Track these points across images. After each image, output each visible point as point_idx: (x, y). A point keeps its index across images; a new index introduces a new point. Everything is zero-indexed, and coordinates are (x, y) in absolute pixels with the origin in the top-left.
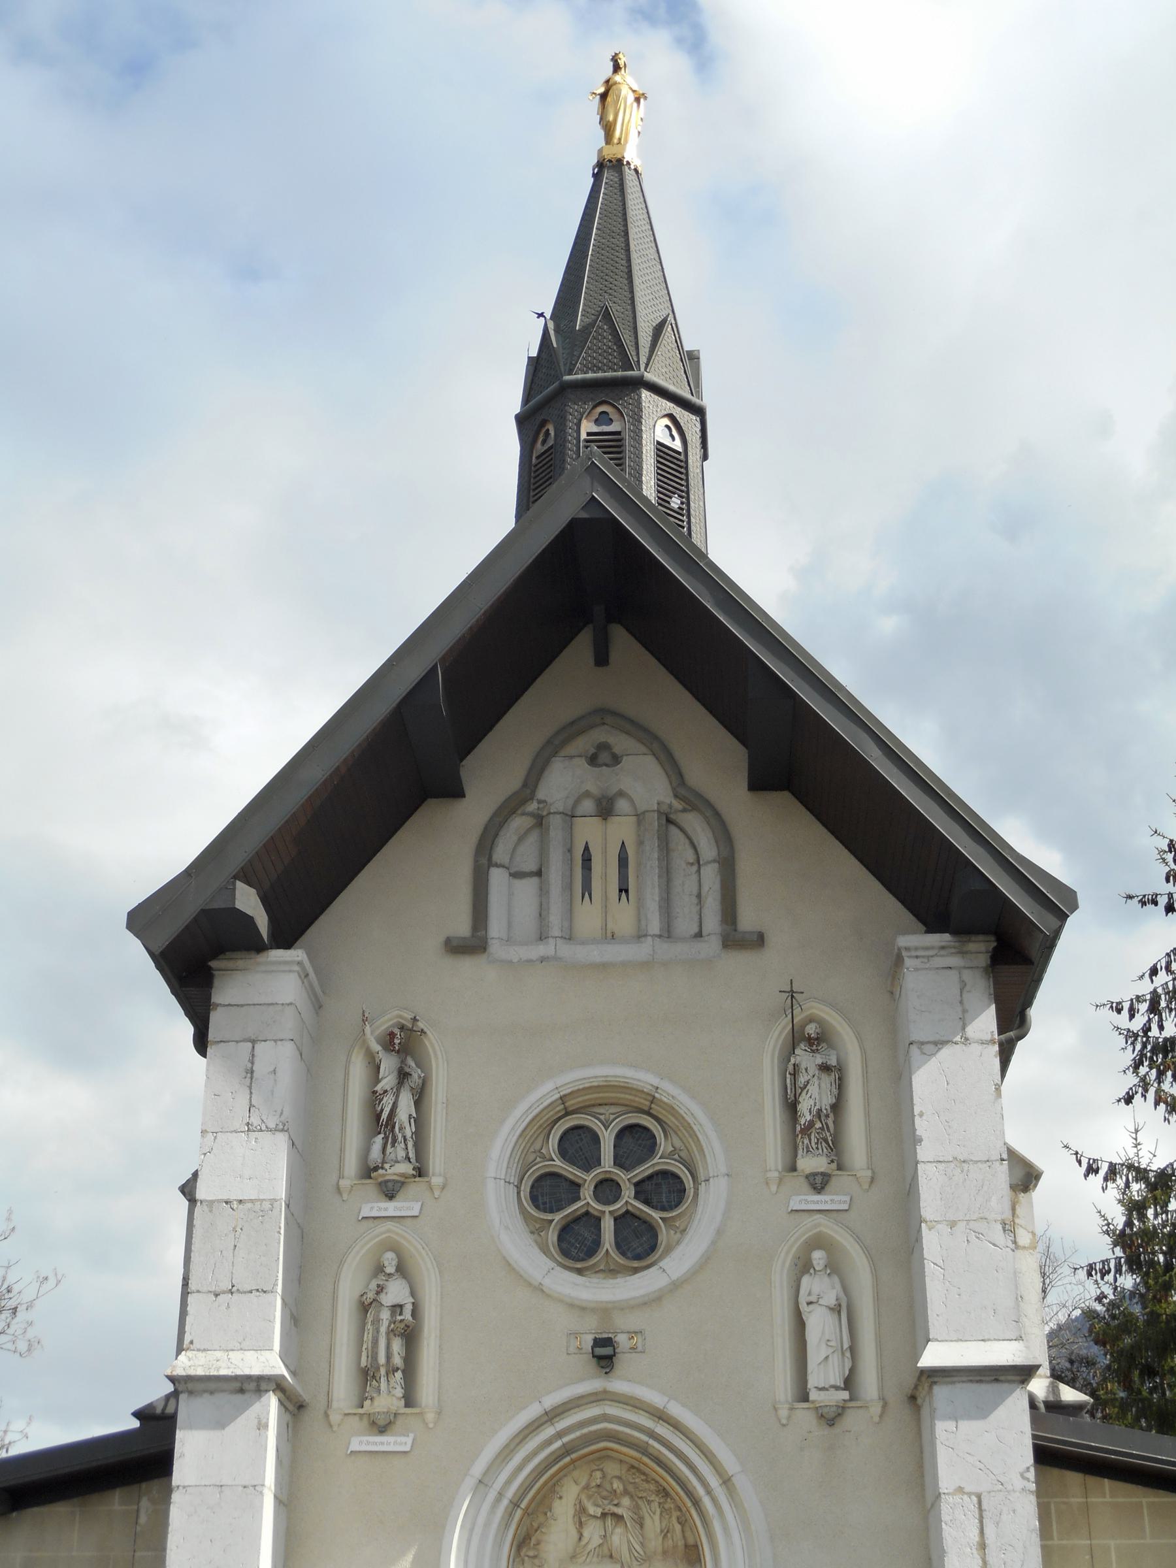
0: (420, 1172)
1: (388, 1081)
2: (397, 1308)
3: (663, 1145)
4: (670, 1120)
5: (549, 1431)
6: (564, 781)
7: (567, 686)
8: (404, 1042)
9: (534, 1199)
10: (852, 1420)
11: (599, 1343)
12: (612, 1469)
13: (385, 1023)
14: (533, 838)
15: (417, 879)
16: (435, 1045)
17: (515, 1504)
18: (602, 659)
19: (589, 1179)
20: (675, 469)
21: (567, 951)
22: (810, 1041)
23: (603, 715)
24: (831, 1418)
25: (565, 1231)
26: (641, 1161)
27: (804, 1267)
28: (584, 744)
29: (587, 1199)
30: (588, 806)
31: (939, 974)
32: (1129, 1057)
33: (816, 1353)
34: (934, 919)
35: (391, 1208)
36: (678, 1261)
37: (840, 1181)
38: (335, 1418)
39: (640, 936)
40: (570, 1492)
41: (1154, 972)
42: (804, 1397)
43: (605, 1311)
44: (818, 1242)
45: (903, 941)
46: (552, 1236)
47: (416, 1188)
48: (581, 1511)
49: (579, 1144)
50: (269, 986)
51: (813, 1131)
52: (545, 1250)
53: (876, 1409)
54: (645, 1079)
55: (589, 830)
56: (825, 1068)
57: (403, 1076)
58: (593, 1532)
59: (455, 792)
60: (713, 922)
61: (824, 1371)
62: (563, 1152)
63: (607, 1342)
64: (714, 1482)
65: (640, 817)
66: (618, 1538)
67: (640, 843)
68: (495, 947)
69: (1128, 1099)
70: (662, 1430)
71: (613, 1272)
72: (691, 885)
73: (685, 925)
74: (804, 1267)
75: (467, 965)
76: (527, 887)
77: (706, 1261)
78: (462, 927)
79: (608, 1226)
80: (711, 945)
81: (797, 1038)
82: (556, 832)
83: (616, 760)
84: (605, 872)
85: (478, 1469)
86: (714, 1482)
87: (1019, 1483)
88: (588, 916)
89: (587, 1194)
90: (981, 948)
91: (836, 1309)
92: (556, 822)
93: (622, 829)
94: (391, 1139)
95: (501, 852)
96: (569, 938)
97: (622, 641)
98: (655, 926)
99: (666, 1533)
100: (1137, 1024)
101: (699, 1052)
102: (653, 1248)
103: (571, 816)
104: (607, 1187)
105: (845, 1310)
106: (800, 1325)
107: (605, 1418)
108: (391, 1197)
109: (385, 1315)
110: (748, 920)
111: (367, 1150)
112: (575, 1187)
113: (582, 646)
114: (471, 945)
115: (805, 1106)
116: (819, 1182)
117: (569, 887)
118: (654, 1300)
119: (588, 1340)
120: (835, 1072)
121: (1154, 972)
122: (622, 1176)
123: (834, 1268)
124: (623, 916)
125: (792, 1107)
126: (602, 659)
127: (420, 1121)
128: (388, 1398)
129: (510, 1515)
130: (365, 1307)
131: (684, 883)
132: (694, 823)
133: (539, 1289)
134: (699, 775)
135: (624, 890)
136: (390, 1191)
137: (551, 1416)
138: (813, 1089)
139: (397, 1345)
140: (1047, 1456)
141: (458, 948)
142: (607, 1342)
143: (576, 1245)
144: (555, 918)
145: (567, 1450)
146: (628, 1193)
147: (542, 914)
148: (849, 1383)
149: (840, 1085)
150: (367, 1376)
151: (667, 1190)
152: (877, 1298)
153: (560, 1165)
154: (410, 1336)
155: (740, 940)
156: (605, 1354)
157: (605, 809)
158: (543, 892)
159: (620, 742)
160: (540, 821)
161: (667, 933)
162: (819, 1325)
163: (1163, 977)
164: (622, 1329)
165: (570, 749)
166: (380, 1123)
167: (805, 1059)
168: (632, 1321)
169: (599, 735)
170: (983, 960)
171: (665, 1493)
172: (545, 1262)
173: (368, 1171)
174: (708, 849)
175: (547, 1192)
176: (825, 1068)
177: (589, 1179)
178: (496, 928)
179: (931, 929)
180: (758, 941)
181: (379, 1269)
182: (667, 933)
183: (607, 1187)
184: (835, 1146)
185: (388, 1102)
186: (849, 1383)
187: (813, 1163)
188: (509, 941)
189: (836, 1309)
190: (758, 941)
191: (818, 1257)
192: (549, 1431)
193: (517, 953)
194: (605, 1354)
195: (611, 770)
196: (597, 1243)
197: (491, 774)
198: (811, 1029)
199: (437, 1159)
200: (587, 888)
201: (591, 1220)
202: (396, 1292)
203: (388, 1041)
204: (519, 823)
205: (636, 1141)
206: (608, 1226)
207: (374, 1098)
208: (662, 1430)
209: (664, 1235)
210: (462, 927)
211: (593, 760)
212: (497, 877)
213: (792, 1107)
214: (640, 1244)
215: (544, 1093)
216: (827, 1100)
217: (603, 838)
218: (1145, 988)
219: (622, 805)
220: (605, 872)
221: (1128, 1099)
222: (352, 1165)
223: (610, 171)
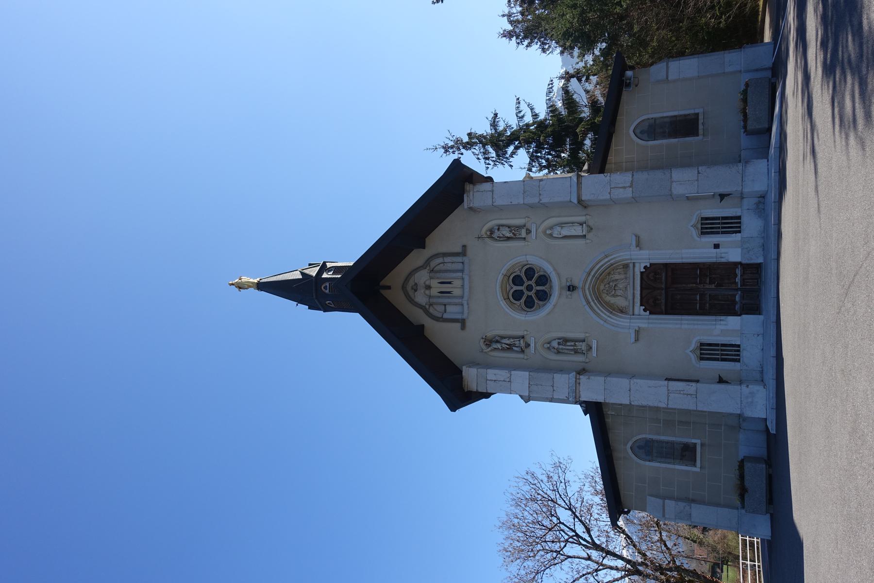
0: (523, 337)
1: (499, 346)
2: (559, 344)
3: (518, 273)
4: (511, 271)
5: (592, 303)
6: (421, 298)
7: (396, 297)
8: (489, 342)
9: (531, 307)
10: (591, 224)
11: (569, 290)
12: (602, 287)
13: (484, 347)
14: (435, 306)
15: (444, 337)
16: (490, 334)
17: (611, 313)
18: (389, 288)
19: (526, 293)
20: (337, 270)
21: (466, 298)
22: (491, 234)
23: (404, 287)
24: (590, 229)
25: (540, 299)
26: (522, 279)
27: (551, 235)
28: (411, 293)
29: (532, 293)
30: (427, 292)
31: (475, 197)
32: (500, 166)
33: (573, 233)
34: (458, 200)
35: (532, 345)
36: (549, 269)
37: (528, 226)
38: (587, 360)
39: (463, 279)
40: (608, 298)
41: (478, 159)
42: (585, 236)
43: (561, 288)
44: (544, 232)
45: (466, 207)
46: (541, 303)
47: (527, 339)
48: (614, 296)
49: (517, 295)
50: (472, 377)
51: (515, 234)
52: (544, 305)
53: (588, 217)
54: (500, 277)
55: (434, 292)
56: (498, 229)
57: (497, 342)
58: (619, 293)
59: (423, 326)
60: (459, 259)
61: (578, 231)
62: (519, 300)
63: (569, 287)
64: (606, 260)
65: (431, 278)
66: (621, 286)
67: (438, 278)
68: (464, 317)
69: (511, 166)
70: (592, 274)
71: (551, 287)
72: (449, 265)
73: (460, 266)
74: (551, 235)
75: (468, 324)
76: (449, 308)
77: (551, 264)
78: (458, 325)
79: (539, 288)
80: (465, 259)
81: (491, 237)
82: (435, 300)
83: (416, 284)
84: (445, 288)
85: (602, 322)
86: (606, 260)
87: (608, 178)
88: (457, 292)
89: (530, 294)
90: (468, 187)
91: (562, 227)
92: (432, 300)
93: (434, 283)
94: (514, 345)
95: (440, 315)
96: (462, 297)
97: (385, 282)
98: (460, 274)
99: (619, 274)
100: (492, 163)
101: (492, 265)
102: (544, 276)
103: (430, 297)
104: (529, 288)
105: (561, 225)
106: (565, 237)
107: (589, 289)
108: (529, 345)
109: (561, 347)
110: (458, 249)
111: (517, 352)
112: (529, 297)
113: (385, 293)
114: (463, 323)
115: (508, 235)
116: (529, 232)
117: (449, 297)
118: (558, 275)
119: (568, 293)
120: (499, 227)
121: (478, 159)
122: (526, 284)
123: (551, 228)
124: (457, 283)
125: (509, 239)
126: (389, 288)
127: (509, 337)
128: (583, 346)
129: (614, 314)
130: (558, 352)
131: (449, 266)
132: (433, 263)
133: (555, 306)
134: (420, 262)
135: (450, 283)
136: (528, 345)
137: (588, 303)
138: (504, 233)
139: (568, 344)
140: (602, 171)
141: (463, 327)
142: (569, 287)
143: (544, 296)
144: (457, 301)
145: (597, 299)
146: (530, 283)
147: (456, 304)
148: (581, 224)
149: (503, 226)
150: (576, 352)
151: (530, 272)
152: (559, 216)
153: (523, 300)
154: (566, 340)
155: (463, 253)
156: (571, 288)
157: (428, 287)
158: (450, 304)
159: (411, 283)
160: (431, 305)
161: (462, 271)
162: (565, 232)
163: (480, 157)
164: (564, 283)
165: (412, 296)
166: (510, 348)
167: (495, 235)
168: (564, 281)
169: (409, 288)
170: (471, 186)
171: (609, 274)
172: (548, 304)
173: (523, 351)
174: (440, 260)
175: (529, 304)
176: (498, 229)
177: (526, 293)
178: (459, 317)
179: (463, 201)
180: (464, 247)
181: (548, 348)
182: (462, 271)
183: (529, 288)
184: (520, 227)
185: (504, 346)
186: (581, 224)
187: (523, 233)
188: (462, 313)
189: (562, 227)
190: (464, 247)
191: (548, 232)
192: (592, 303)
193: (466, 311)
194: (571, 288)
195: (414, 283)
196: (543, 291)
197: (417, 316)
198: (488, 233)
199: (520, 333)
200: (449, 292)
201: (530, 278)
202: (555, 344)
203: (488, 345)
204: (431, 310)
205: (517, 280)
206: (539, 288)
207: (503, 349)
208: (592, 274)
209: (542, 273)
210: (458, 325)
211: (416, 291)
212: (446, 316)
213: (509, 239)
214: (544, 280)
215: (503, 304)
216: (507, 229)
217: (436, 288)
218: (482, 161)
219: (427, 283)
220: (445, 288)
221: (511, 166)
222: (521, 356)
223: (261, 286)
